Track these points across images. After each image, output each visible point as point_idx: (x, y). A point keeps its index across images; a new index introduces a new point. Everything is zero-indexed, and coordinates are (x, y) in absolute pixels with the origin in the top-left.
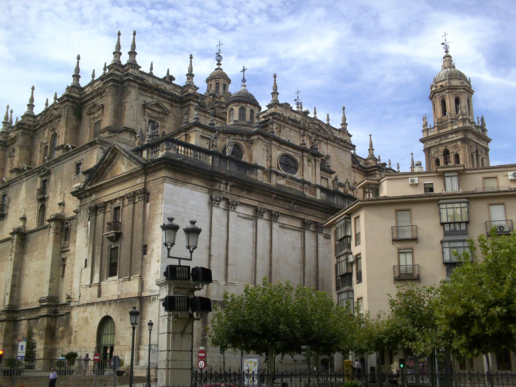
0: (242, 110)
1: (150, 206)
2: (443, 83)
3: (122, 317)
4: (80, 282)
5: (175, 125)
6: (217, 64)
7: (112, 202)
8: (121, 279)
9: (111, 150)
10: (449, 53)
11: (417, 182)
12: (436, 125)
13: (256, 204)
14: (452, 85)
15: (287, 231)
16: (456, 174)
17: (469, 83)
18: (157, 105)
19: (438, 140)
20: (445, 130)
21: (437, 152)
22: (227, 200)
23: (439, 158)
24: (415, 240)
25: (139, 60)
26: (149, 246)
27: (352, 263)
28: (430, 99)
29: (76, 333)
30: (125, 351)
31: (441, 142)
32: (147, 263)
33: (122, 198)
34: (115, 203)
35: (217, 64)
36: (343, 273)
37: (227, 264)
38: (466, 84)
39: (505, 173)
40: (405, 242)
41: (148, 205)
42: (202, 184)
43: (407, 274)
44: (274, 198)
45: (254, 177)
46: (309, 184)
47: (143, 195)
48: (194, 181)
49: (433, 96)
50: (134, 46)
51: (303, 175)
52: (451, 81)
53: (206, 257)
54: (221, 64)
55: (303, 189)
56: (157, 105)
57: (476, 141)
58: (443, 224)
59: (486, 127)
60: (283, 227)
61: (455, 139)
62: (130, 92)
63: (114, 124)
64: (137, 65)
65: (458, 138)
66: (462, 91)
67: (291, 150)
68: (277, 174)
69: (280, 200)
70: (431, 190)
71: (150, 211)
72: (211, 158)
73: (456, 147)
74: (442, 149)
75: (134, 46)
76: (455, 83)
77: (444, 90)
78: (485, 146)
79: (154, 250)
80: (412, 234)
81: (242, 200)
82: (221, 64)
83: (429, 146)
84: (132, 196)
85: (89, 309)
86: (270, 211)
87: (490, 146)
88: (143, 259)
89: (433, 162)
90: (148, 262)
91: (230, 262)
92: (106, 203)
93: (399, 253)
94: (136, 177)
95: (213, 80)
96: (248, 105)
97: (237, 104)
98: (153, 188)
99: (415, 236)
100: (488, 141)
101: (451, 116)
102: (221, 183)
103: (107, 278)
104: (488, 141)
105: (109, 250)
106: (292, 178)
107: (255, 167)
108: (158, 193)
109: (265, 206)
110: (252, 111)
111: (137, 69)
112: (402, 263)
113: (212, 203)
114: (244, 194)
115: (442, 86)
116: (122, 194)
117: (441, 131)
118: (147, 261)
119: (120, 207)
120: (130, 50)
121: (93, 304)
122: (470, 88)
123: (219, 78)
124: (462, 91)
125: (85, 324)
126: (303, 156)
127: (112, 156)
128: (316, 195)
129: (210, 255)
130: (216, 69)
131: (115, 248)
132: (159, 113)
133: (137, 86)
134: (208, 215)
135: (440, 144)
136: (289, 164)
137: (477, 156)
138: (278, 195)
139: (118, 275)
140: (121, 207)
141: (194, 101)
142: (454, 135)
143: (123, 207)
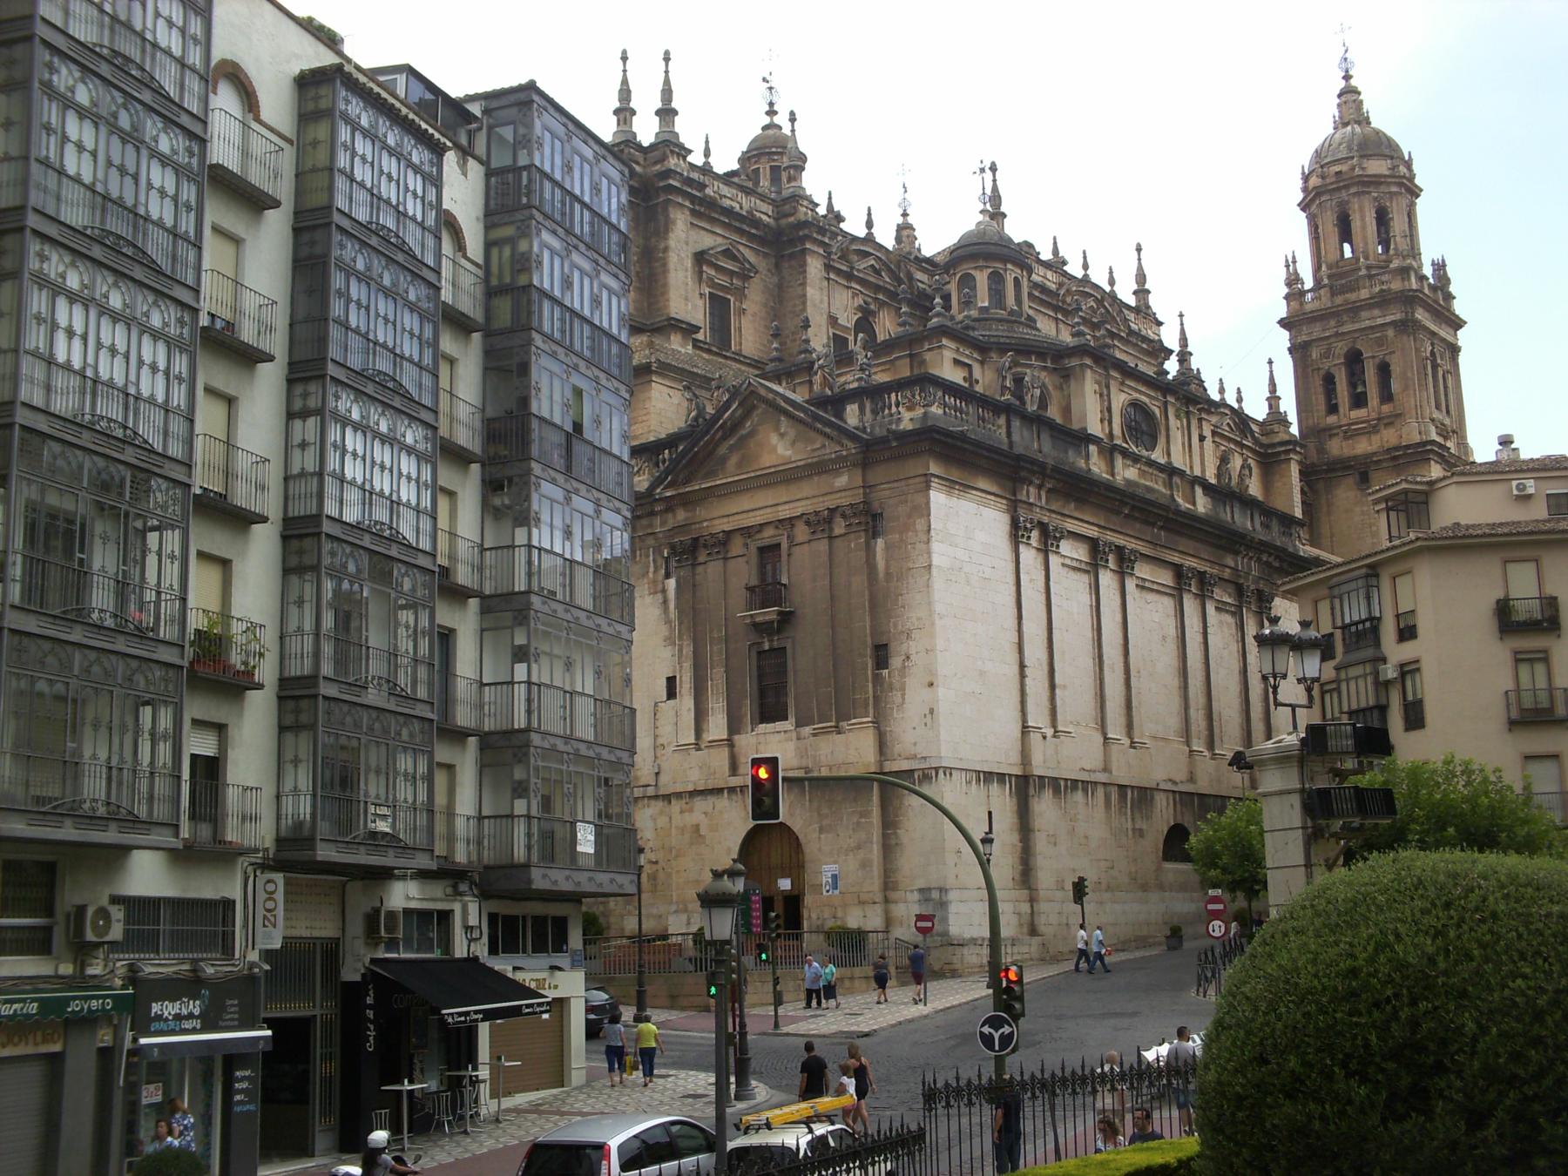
0: (996, 279)
1: (887, 548)
3: (825, 822)
4: (656, 737)
5: (765, 305)
6: (768, 113)
7: (747, 532)
8: (807, 730)
9: (740, 398)
10: (1353, 82)
11: (1531, 491)
12: (1326, 281)
13: (1092, 532)
14: (1370, 172)
15: (1151, 597)
18: (727, 253)
19: (1333, 323)
20: (1352, 296)
21: (1327, 355)
22: (1043, 527)
23: (1334, 371)
25: (688, 131)
26: (893, 646)
27: (1387, 683)
28: (1303, 210)
29: (655, 867)
30: (845, 906)
31: (1341, 330)
33: (791, 521)
34: (758, 536)
35: (768, 113)
36: (1363, 705)
37: (1052, 687)
38: (1403, 170)
41: (880, 543)
42: (994, 489)
43: (1537, 711)
44: (1127, 516)
45: (1082, 463)
46: (1181, 473)
47: (863, 519)
48: (982, 483)
49: (1312, 200)
50: (667, 93)
51: (1169, 455)
52: (1366, 163)
53: (1016, 669)
54: (776, 113)
55: (1171, 488)
56: (727, 253)
57: (1433, 327)
59: (1452, 289)
60: (1143, 588)
61: (1380, 321)
62: (674, 223)
63: (636, 309)
64: (682, 147)
65: (1388, 319)
66: (1394, 189)
67: (1143, 389)
68: (1125, 454)
69: (1136, 519)
72: (1002, 421)
73: (1380, 342)
74: (1341, 348)
75: (667, 93)
76: (1377, 167)
77: (1346, 187)
78: (1450, 339)
81: (1071, 525)
82: (776, 113)
83: (1305, 338)
84: (821, 523)
85: (700, 804)
86: (1120, 550)
87: (1463, 337)
88: (877, 679)
89: (1317, 382)
90: (897, 685)
91: (1057, 681)
92: (728, 534)
93: (1517, 661)
94: (836, 472)
95: (764, 159)
96: (1009, 266)
98: (891, 501)
100: (1458, 324)
101: (1367, 258)
102: (1031, 483)
103: (754, 725)
104: (1458, 324)
105: (754, 654)
106: (1151, 463)
107: (1083, 439)
108: (909, 516)
109: (1111, 537)
110: (1017, 281)
111: (684, 158)
113: (1017, 533)
114: (1070, 509)
116: (785, 512)
117: (1339, 300)
118: (891, 684)
120: (659, 105)
121: (718, 791)
122: (1412, 178)
123: (774, 156)
124: (1394, 189)
125: (691, 844)
126: (1166, 403)
127: (740, 412)
128: (1194, 504)
129: (1022, 666)
130: (764, 128)
131: (772, 650)
132: (731, 273)
133: (687, 203)
134: (1012, 566)
136: (1143, 427)
137: (1435, 366)
138: (1133, 508)
139: (792, 719)
140: (784, 546)
141: (815, 241)
142: (1376, 312)
143: (790, 548)
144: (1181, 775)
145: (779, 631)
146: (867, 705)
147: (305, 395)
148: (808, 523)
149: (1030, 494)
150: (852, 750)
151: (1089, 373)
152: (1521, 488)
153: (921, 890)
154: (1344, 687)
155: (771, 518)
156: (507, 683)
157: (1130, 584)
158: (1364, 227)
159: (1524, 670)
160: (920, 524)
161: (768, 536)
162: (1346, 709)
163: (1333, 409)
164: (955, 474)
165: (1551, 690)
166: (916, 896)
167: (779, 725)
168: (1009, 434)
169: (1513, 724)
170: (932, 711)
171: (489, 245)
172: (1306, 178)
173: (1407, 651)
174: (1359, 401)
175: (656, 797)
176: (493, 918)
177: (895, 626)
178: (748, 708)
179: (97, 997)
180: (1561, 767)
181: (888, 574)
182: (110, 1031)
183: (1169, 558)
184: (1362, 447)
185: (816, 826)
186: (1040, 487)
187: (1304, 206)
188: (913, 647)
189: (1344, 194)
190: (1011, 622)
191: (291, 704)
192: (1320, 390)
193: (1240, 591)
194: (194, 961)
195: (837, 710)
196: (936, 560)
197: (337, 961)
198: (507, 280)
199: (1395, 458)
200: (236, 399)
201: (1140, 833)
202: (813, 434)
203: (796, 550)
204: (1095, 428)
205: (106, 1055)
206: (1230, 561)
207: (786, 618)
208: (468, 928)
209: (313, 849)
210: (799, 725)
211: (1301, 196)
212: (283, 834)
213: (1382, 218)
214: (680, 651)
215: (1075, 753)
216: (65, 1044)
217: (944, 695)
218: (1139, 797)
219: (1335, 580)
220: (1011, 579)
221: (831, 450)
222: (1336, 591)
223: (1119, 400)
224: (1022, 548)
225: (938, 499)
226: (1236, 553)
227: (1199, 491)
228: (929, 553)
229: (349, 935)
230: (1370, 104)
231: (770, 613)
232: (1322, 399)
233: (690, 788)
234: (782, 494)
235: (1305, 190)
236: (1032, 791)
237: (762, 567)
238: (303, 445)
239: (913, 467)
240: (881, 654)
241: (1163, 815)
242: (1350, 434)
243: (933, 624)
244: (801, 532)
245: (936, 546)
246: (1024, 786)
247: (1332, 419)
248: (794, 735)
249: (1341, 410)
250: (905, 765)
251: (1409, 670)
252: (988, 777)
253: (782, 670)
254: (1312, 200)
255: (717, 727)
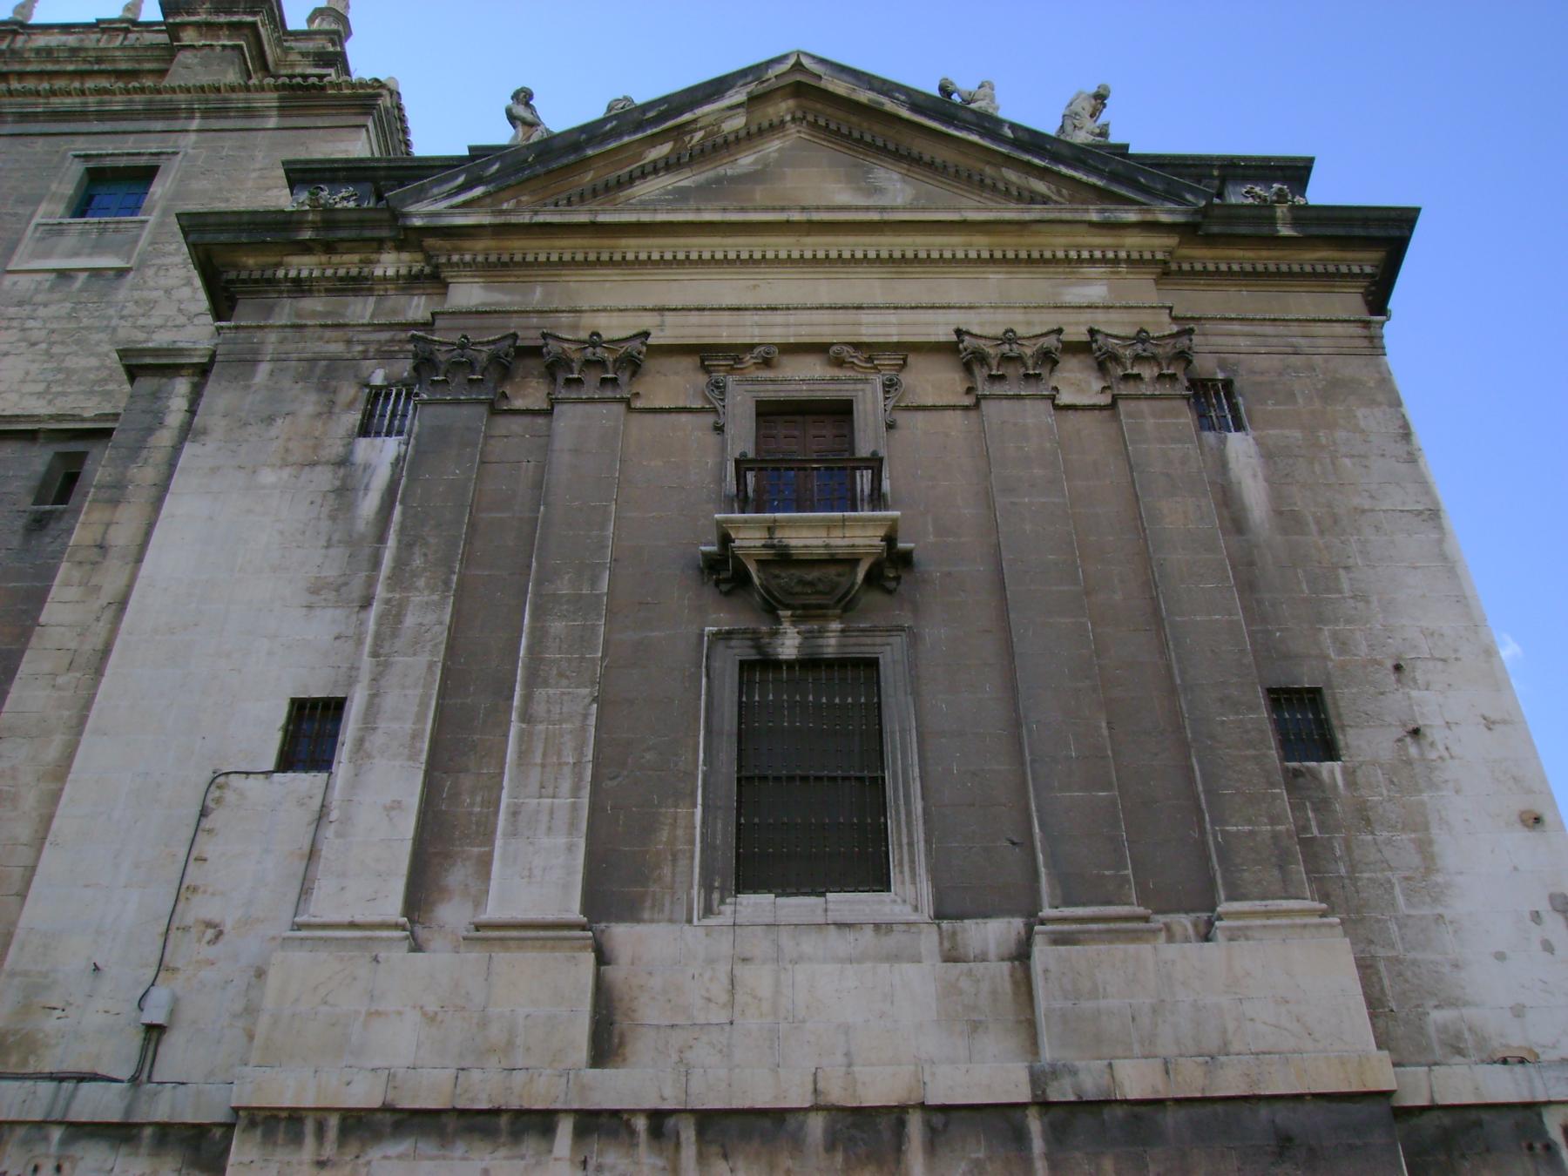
1: (1268, 455)
4: (183, 890)
131: (810, 663)
155: (824, 334)
161: (804, 378)
175: (121, 1133)
177: (1343, 645)
178: (692, 827)
181: (1287, 518)
188: (1437, 702)
189: (540, 169)
194: (771, 528)
210: (949, 908)
214: (393, 617)
233: (363, 1094)
240: (1305, 722)
255: (535, 864)
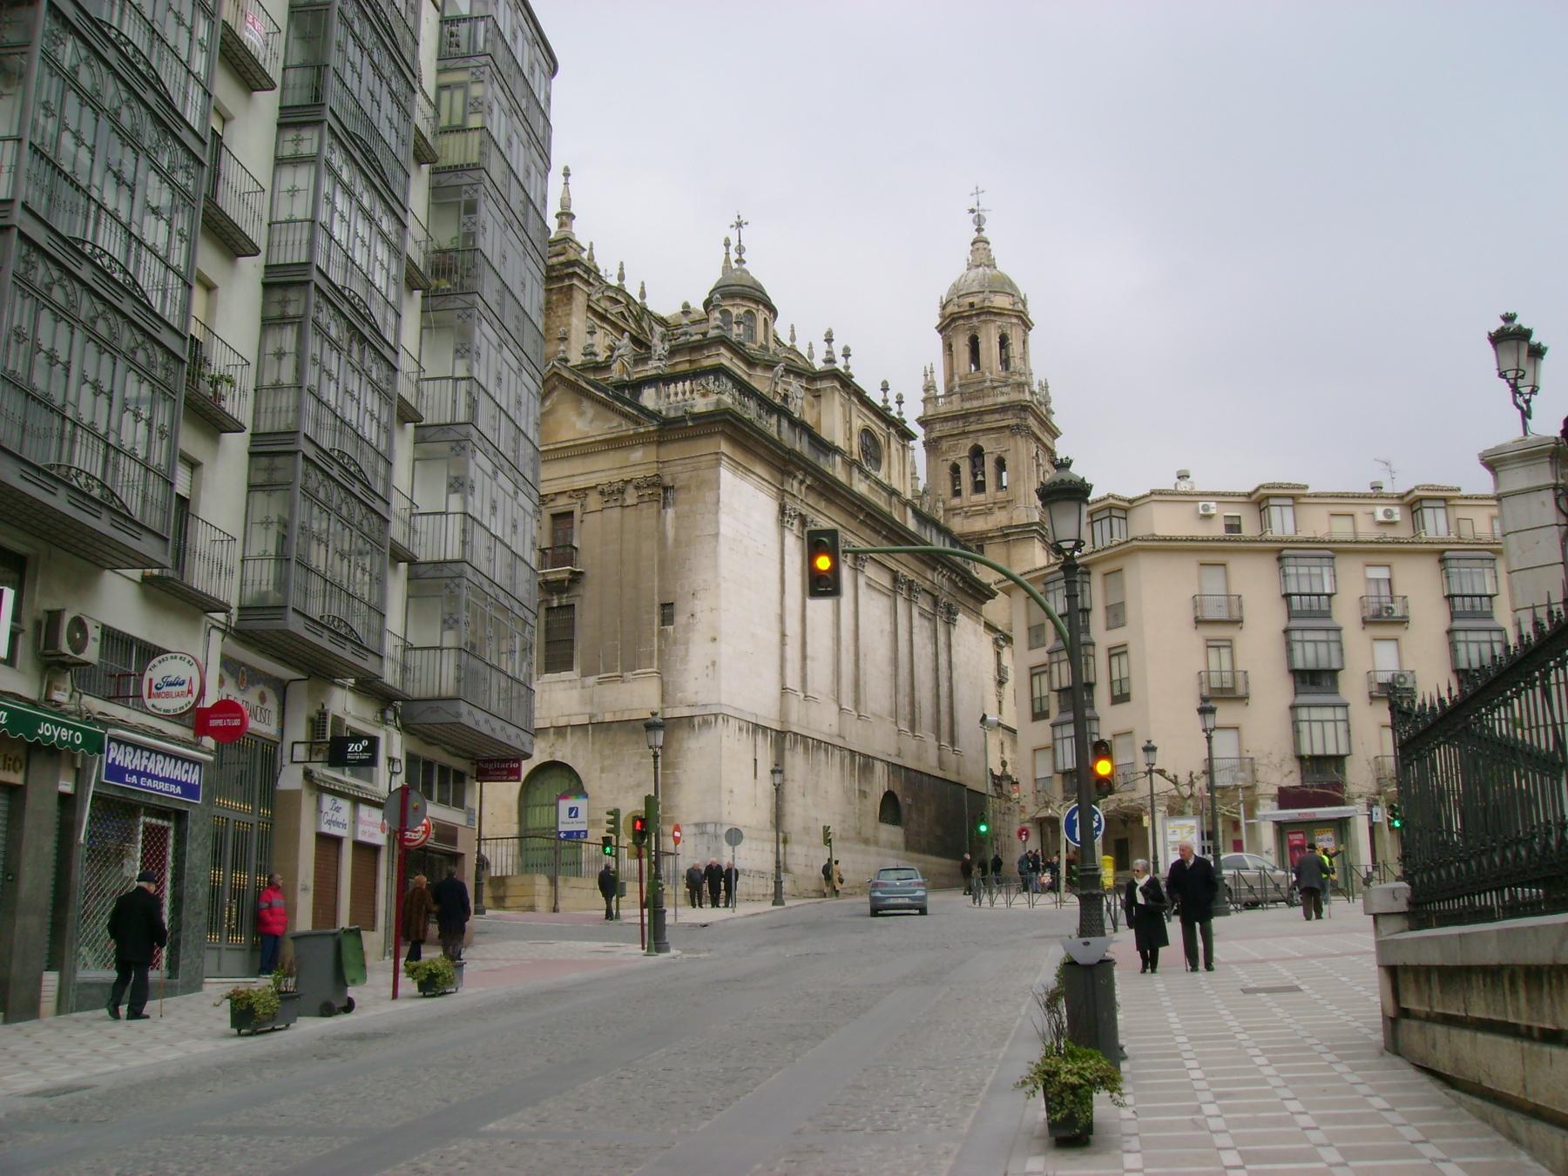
1: (678, 516)
2: (975, 300)
3: (607, 763)
8: (592, 680)
11: (1213, 511)
16: (1290, 502)
17: (1024, 303)
20: (976, 403)
24: (1237, 622)
26: (678, 606)
28: (940, 332)
32: (675, 643)
33: (583, 492)
38: (1020, 307)
39: (1369, 509)
40: (1215, 624)
41: (670, 512)
43: (1222, 690)
45: (830, 471)
48: (759, 469)
49: (949, 325)
53: (776, 637)
58: (1287, 596)
70: (1238, 528)
71: (677, 529)
72: (775, 418)
74: (968, 443)
76: (1001, 302)
79: (698, 615)
80: (1230, 612)
83: (935, 435)
84: (613, 494)
88: (662, 634)
89: (945, 470)
97: (738, 301)
99: (1236, 616)
100: (1055, 434)
106: (878, 482)
112: (1214, 666)
114: (822, 505)
115: (972, 305)
116: (580, 483)
119: (572, 513)
124: (1014, 320)
129: (783, 635)
131: (560, 607)
134: (776, 547)
135: (964, 433)
140: (577, 514)
144: (893, 751)
145: (567, 590)
146: (651, 657)
147: (298, 141)
148: (602, 493)
149: (794, 486)
150: (638, 696)
151: (837, 395)
152: (1206, 508)
153: (696, 825)
154: (1055, 667)
156: (441, 513)
157: (862, 581)
158: (990, 348)
159: (1213, 653)
160: (709, 497)
161: (562, 504)
162: (1056, 686)
163: (957, 493)
164: (739, 457)
165: (1233, 671)
166: (693, 830)
167: (565, 675)
168: (779, 432)
169: (1366, 622)
170: (714, 664)
171: (441, 88)
172: (944, 307)
173: (1116, 637)
174: (979, 487)
176: (412, 759)
177: (682, 586)
179: (68, 727)
180: (1239, 738)
182: (72, 775)
183: (888, 564)
184: (979, 525)
185: (598, 766)
186: (802, 482)
187: (942, 329)
188: (701, 606)
190: (776, 596)
191: (264, 461)
192: (948, 477)
193: (935, 602)
195: (625, 659)
196: (723, 530)
197: (274, 767)
198: (457, 121)
199: (1007, 535)
200: (232, 118)
201: (863, 794)
202: (610, 414)
203: (588, 518)
204: (840, 442)
205: (67, 802)
206: (929, 575)
207: (576, 577)
208: (391, 760)
209: (283, 618)
210: (584, 675)
211: (938, 321)
212: (247, 603)
213: (1004, 341)
215: (822, 720)
216: (26, 780)
217: (725, 649)
218: (863, 764)
219: (1050, 578)
220: (777, 557)
221: (627, 428)
222: (1051, 587)
223: (858, 424)
224: (787, 533)
225: (726, 476)
226: (934, 569)
227: (909, 512)
228: (717, 522)
229: (290, 736)
230: (996, 250)
231: (562, 572)
232: (948, 484)
234: (577, 466)
235: (943, 316)
236: (787, 745)
237: (554, 531)
238: (293, 192)
239: (705, 446)
240: (667, 611)
241: (880, 782)
242: (969, 514)
243: (718, 586)
244: (594, 501)
245: (724, 518)
246: (781, 738)
247: (956, 502)
248: (579, 684)
249: (964, 493)
250: (686, 712)
251: (1117, 652)
252: (757, 728)
253: (570, 626)
254: (949, 325)
